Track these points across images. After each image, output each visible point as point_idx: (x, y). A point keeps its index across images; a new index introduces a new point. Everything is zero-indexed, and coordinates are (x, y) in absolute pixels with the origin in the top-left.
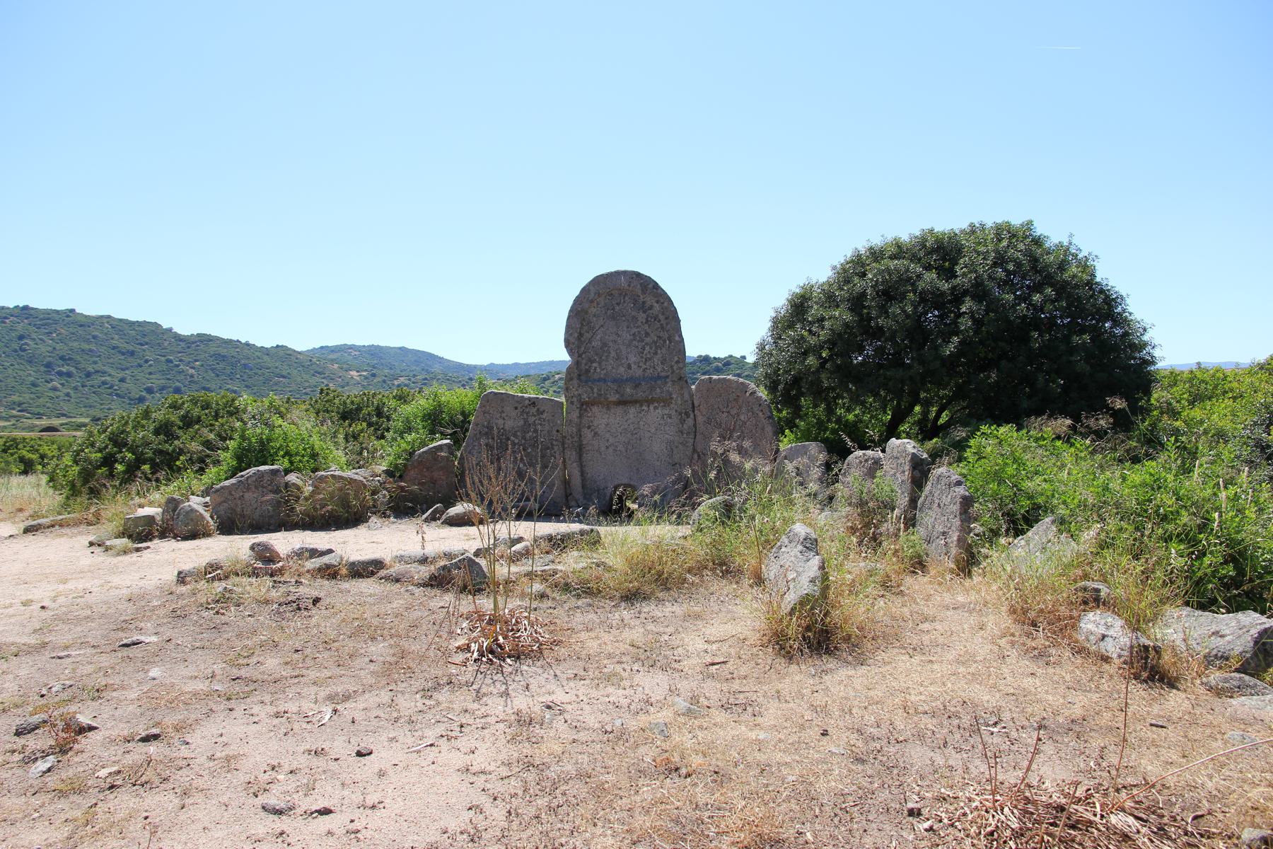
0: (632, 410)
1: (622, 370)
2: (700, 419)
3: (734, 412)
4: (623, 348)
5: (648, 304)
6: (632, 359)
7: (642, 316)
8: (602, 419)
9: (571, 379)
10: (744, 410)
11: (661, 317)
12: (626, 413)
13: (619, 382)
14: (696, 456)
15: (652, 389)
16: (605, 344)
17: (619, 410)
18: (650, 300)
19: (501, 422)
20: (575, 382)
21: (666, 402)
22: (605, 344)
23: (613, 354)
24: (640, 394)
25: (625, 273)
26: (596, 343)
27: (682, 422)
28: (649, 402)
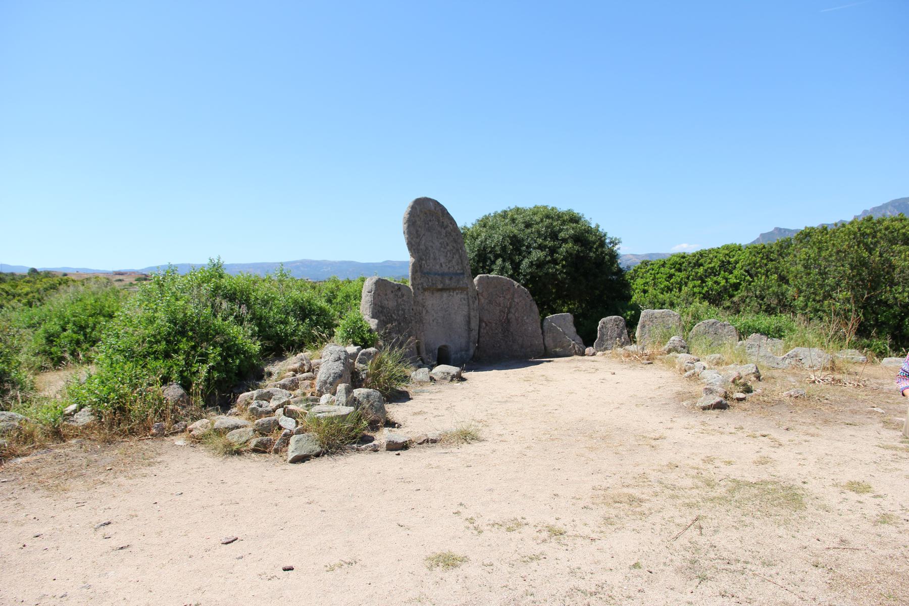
0: (445, 295)
1: (438, 267)
2: (483, 301)
3: (508, 297)
4: (437, 252)
5: (445, 223)
6: (442, 260)
7: (444, 231)
8: (433, 302)
9: (416, 272)
10: (516, 295)
11: (453, 234)
12: (442, 297)
13: (443, 275)
14: (484, 324)
15: (458, 281)
16: (427, 248)
17: (438, 295)
18: (446, 222)
19: (386, 302)
20: (419, 274)
21: (463, 289)
22: (427, 248)
23: (432, 256)
24: (453, 285)
25: (430, 199)
26: (422, 247)
27: (474, 302)
28: (454, 289)
